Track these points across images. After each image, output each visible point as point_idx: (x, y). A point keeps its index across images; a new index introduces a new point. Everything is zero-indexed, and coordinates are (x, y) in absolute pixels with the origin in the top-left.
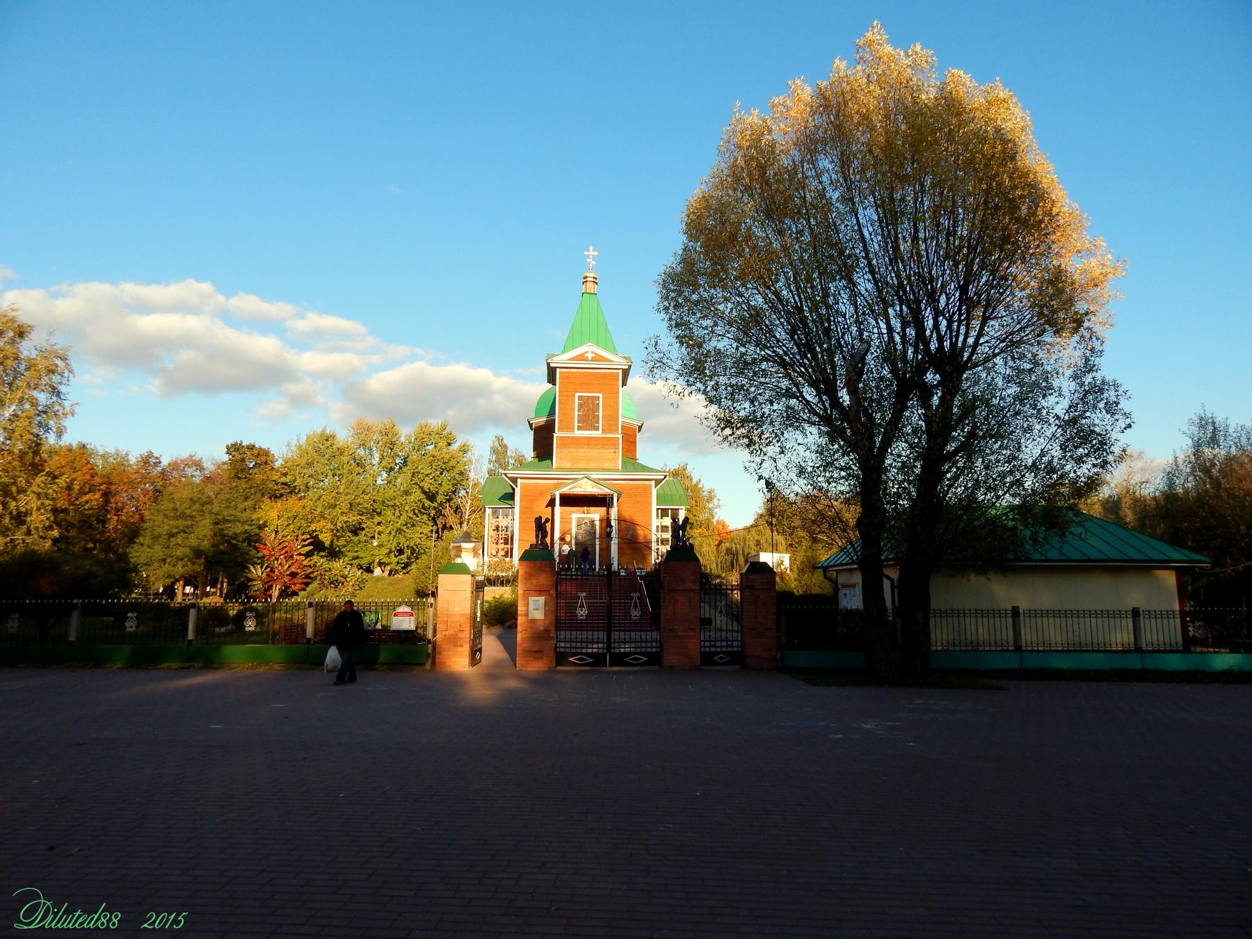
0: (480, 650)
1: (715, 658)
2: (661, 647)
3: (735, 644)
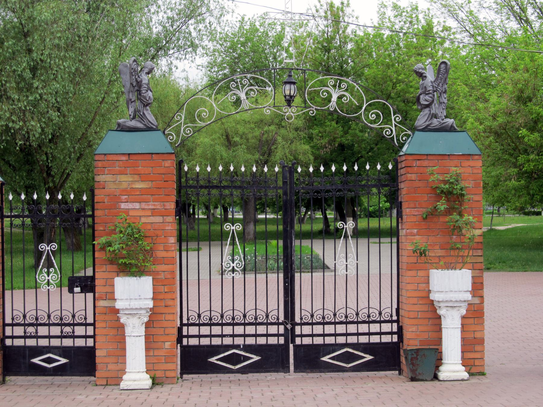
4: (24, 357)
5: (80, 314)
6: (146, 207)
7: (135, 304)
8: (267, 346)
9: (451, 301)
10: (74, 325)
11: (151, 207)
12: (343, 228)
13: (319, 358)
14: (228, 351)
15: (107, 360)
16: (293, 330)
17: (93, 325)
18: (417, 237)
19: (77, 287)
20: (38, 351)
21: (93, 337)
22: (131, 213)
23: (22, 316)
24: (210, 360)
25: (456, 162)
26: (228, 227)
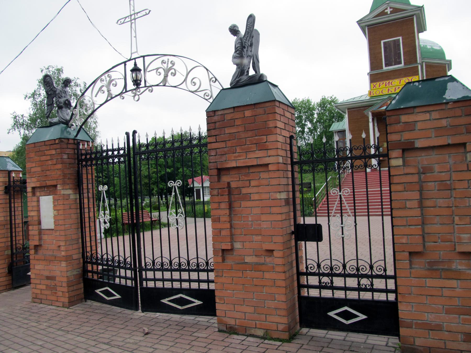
5: (379, 265)
10: (372, 277)
12: (173, 186)
17: (394, 277)
21: (395, 291)
23: (316, 265)
24: (201, 303)
26: (171, 184)
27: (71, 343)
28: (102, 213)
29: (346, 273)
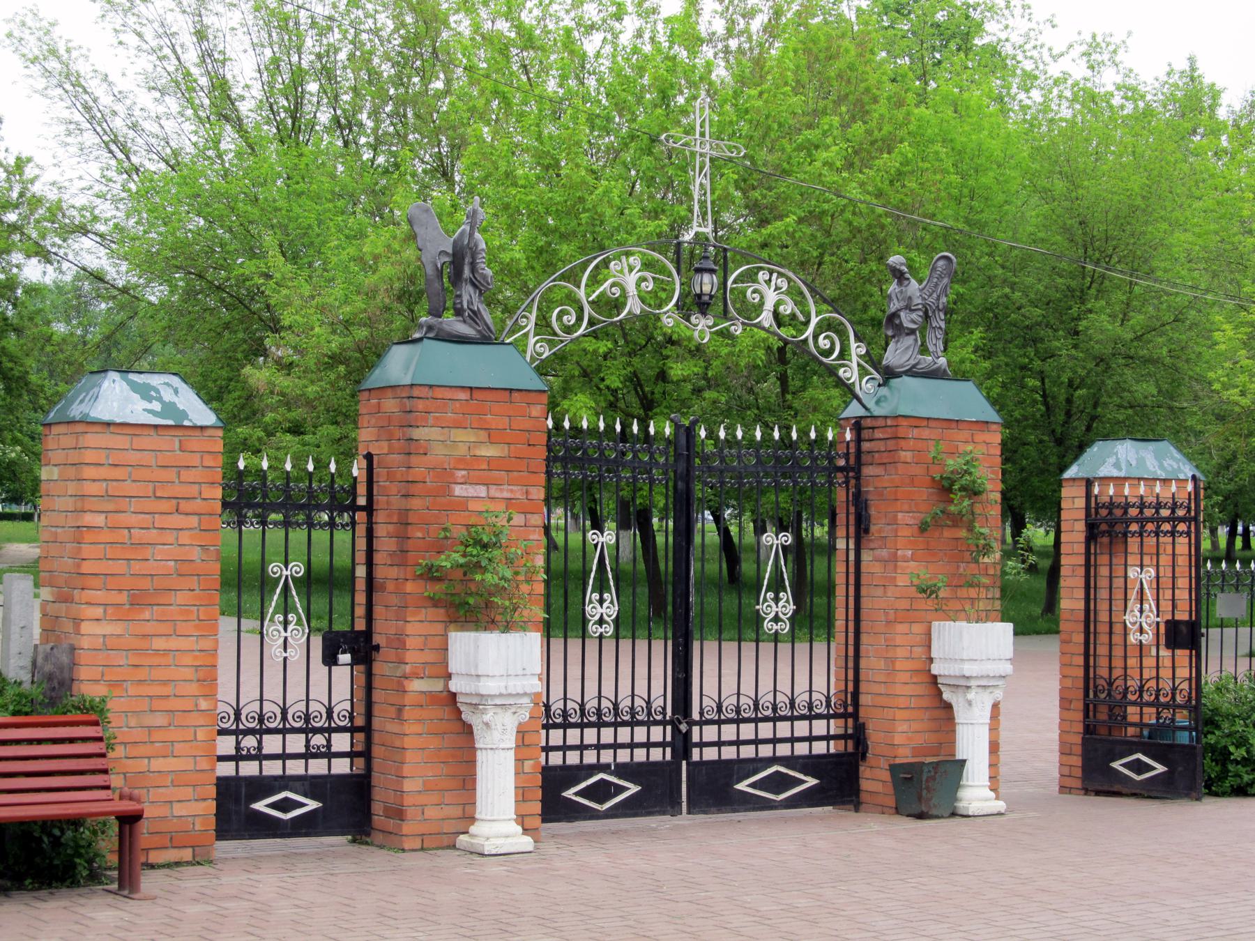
0: (991, 766)
1: (1116, 765)
2: (363, 754)
3: (657, 734)
4: (237, 800)
6: (498, 495)
7: (517, 685)
8: (649, 766)
9: (988, 676)
11: (506, 495)
12: (281, 576)
13: (729, 785)
14: (591, 776)
15: (422, 799)
16: (688, 735)
18: (912, 564)
19: (344, 652)
20: (263, 786)
22: (472, 506)
25: (965, 434)
27: (253, 938)
28: (1133, 605)
29: (333, 725)
